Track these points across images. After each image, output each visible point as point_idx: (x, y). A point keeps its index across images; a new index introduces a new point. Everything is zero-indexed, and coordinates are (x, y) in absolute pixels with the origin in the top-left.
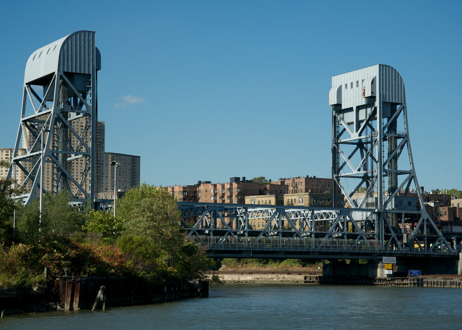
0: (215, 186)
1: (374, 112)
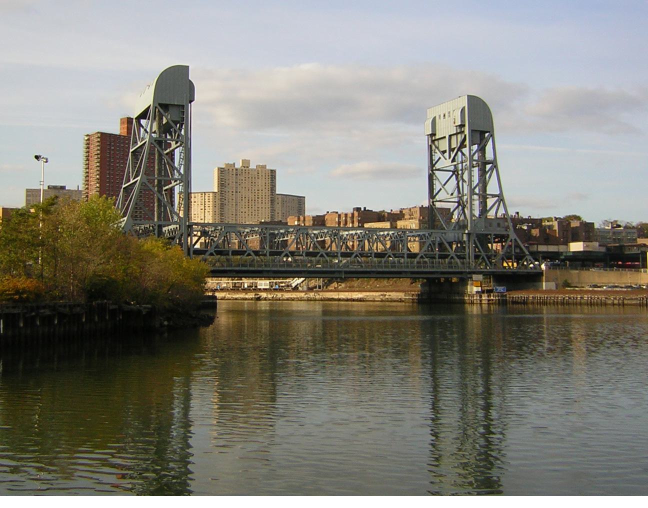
0: (340, 216)
1: (464, 140)
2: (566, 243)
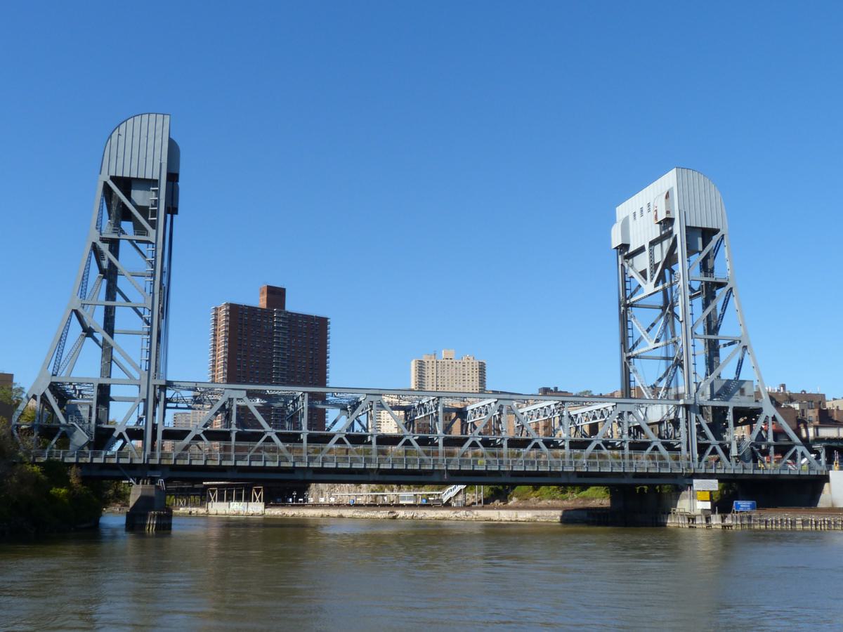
1: (674, 246)
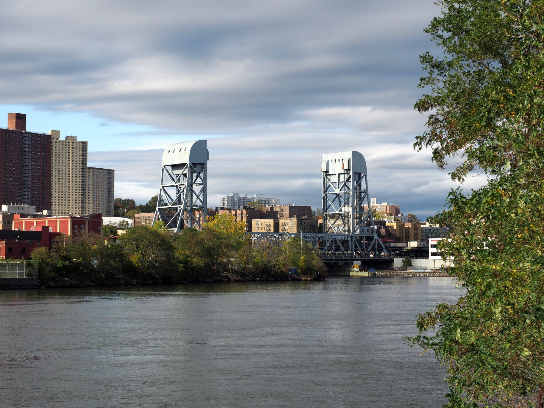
2: (406, 242)
